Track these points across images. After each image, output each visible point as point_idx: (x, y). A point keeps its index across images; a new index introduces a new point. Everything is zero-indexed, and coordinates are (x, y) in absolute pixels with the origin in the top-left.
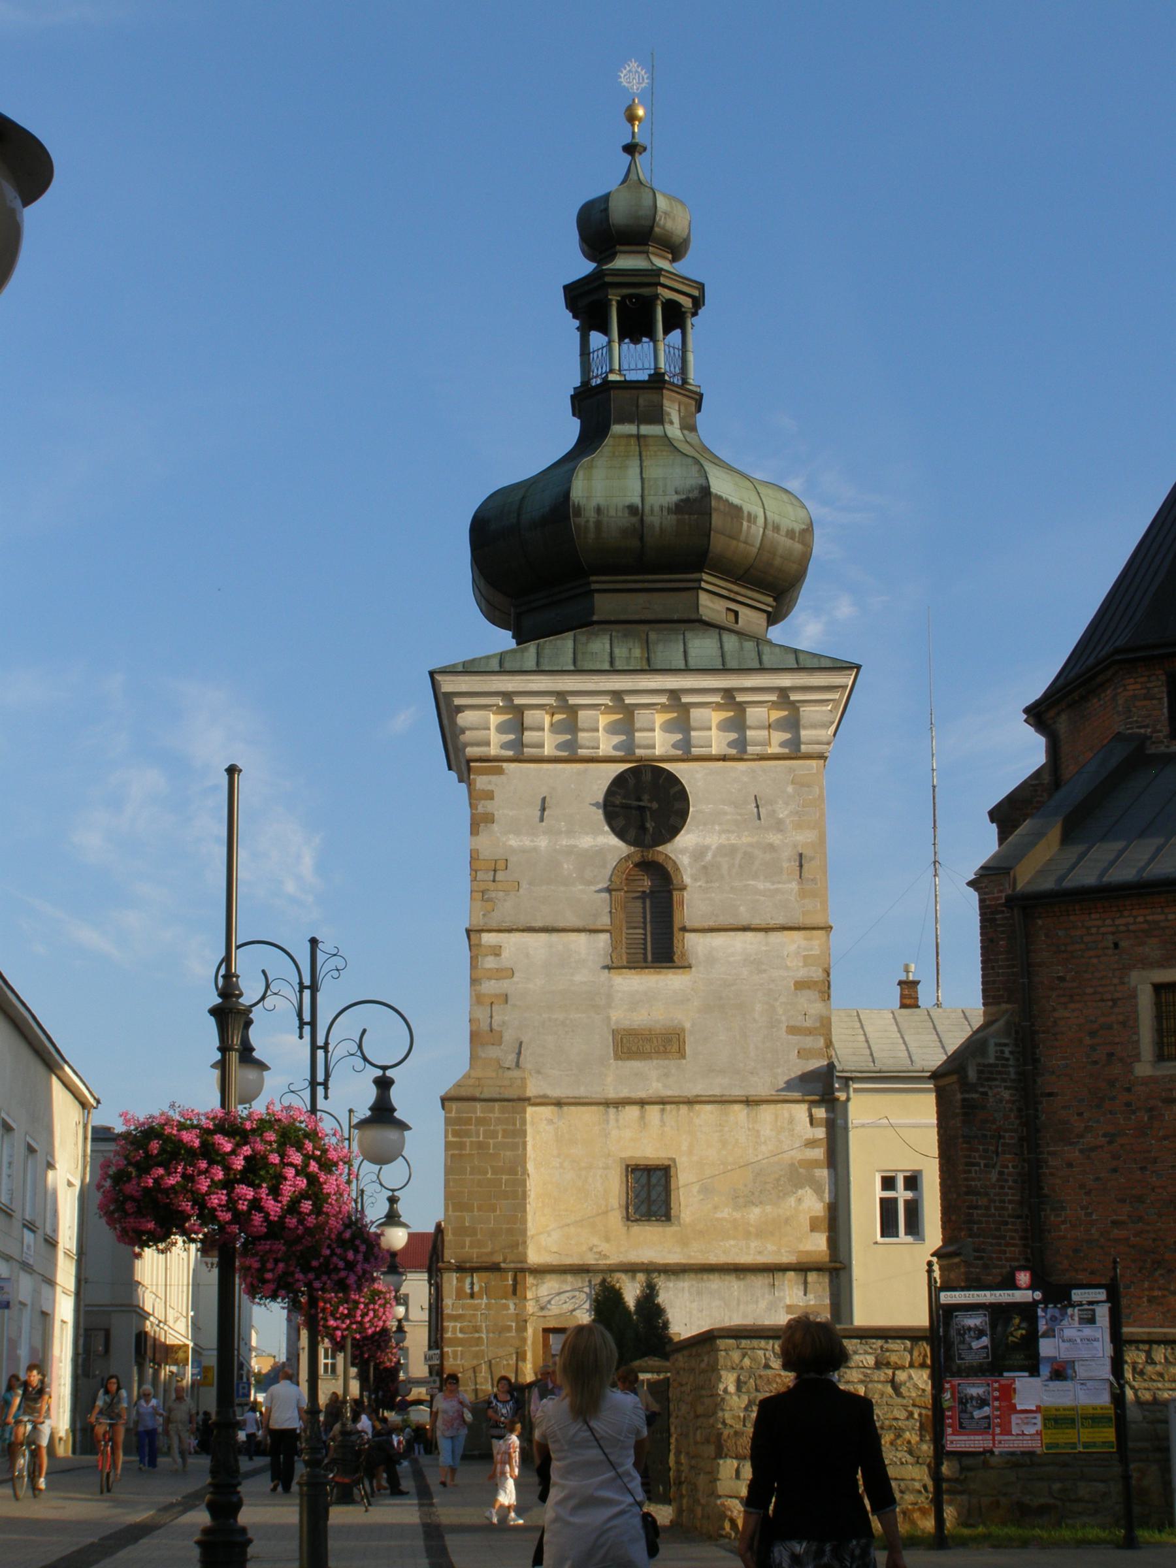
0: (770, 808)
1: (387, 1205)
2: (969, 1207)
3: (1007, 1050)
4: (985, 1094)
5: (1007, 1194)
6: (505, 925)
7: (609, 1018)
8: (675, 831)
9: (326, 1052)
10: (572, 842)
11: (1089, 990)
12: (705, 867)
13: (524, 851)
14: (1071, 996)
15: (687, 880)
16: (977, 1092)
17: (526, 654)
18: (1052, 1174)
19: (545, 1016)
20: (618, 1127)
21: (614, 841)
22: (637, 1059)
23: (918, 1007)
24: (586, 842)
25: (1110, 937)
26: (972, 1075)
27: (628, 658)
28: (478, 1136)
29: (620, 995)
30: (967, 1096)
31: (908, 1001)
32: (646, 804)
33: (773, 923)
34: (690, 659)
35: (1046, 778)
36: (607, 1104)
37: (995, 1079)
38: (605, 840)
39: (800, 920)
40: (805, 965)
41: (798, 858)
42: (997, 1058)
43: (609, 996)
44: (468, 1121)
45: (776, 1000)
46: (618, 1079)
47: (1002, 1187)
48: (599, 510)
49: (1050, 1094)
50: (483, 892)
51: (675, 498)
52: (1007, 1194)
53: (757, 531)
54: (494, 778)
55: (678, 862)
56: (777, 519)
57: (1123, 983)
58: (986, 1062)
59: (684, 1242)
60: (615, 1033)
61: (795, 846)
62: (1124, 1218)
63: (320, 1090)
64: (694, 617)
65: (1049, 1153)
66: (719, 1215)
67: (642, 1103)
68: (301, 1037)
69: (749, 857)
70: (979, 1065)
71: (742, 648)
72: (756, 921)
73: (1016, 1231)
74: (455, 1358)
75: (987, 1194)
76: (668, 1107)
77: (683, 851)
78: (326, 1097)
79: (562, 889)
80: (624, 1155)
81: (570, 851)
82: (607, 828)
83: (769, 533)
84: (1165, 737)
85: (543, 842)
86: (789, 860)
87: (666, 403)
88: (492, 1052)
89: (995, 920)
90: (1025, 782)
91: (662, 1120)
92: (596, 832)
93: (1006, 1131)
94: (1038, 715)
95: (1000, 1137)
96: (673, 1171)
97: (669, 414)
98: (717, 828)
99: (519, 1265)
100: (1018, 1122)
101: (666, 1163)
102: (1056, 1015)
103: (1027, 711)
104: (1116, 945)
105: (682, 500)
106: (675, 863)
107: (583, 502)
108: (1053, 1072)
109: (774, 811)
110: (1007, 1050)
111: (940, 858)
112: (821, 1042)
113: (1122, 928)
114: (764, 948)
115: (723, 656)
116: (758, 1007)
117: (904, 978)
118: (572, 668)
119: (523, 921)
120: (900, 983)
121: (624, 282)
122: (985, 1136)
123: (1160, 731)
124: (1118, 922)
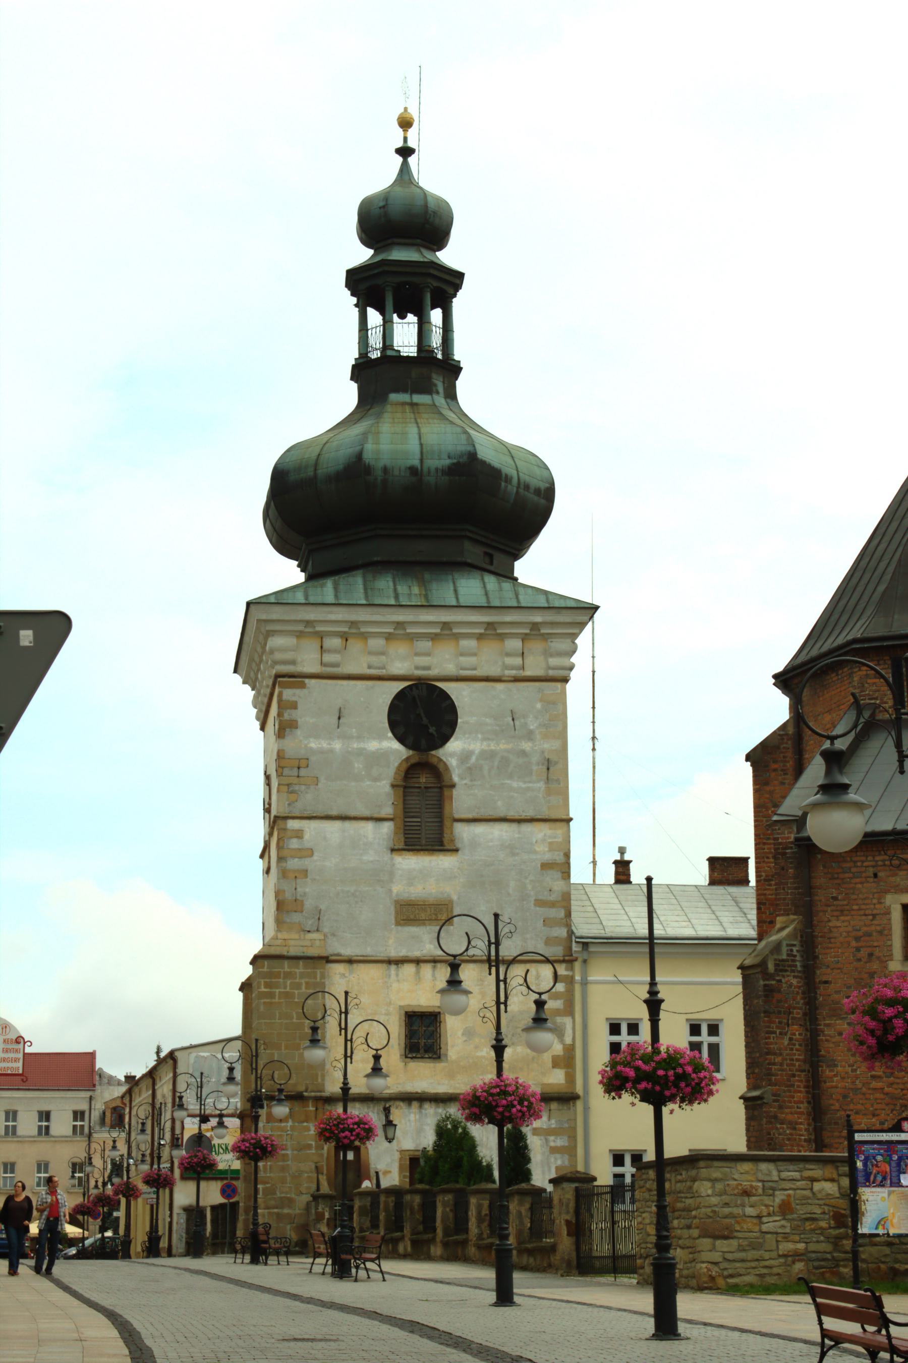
0: (522, 720)
1: (372, 1060)
2: (769, 1064)
3: (795, 949)
4: (780, 981)
5: (795, 1055)
6: (306, 814)
7: (390, 891)
8: (446, 739)
9: (505, 984)
10: (362, 745)
11: (855, 907)
12: (470, 768)
13: (322, 752)
14: (842, 911)
15: (456, 779)
16: (774, 980)
17: (325, 589)
18: (827, 1040)
19: (339, 888)
20: (398, 981)
21: (396, 745)
22: (413, 926)
23: (630, 883)
24: (373, 745)
25: (871, 869)
26: (771, 967)
27: (410, 595)
28: (285, 987)
29: (400, 872)
30: (767, 982)
31: (622, 877)
32: (423, 715)
33: (524, 815)
34: (460, 597)
35: (791, 730)
36: (389, 962)
37: (786, 971)
38: (389, 745)
39: (545, 813)
40: (550, 850)
41: (546, 763)
42: (788, 955)
43: (392, 874)
44: (278, 975)
45: (526, 878)
46: (398, 941)
47: (792, 1049)
48: (385, 470)
49: (826, 982)
50: (288, 785)
51: (447, 462)
52: (795, 1055)
54: (298, 691)
55: (448, 763)
56: (527, 479)
57: (881, 903)
58: (780, 958)
59: (451, 1075)
60: (397, 902)
61: (543, 752)
62: (881, 1073)
63: (349, 1059)
64: (459, 559)
65: (826, 1025)
66: (479, 1054)
67: (418, 962)
68: (490, 974)
69: (505, 761)
70: (775, 960)
71: (501, 589)
72: (512, 814)
73: (801, 1081)
74: (265, 1172)
75: (781, 1054)
76: (439, 965)
77: (452, 755)
78: (506, 1012)
79: (353, 784)
80: (402, 1004)
81: (360, 752)
82: (390, 734)
84: (890, 708)
85: (337, 745)
86: (538, 764)
87: (434, 376)
88: (296, 918)
89: (786, 853)
90: (774, 732)
91: (433, 975)
92: (381, 737)
93: (795, 1008)
94: (784, 680)
95: (790, 1013)
96: (410, 1010)
97: (436, 385)
98: (480, 736)
99: (318, 1094)
100: (802, 1001)
101: (437, 1010)
102: (830, 924)
103: (775, 677)
104: (875, 875)
105: (454, 464)
106: (445, 764)
107: (372, 463)
108: (828, 966)
109: (526, 723)
110: (795, 949)
111: (596, 735)
112: (562, 914)
113: (880, 863)
114: (517, 836)
115: (486, 594)
116: (512, 884)
117: (619, 858)
118: (364, 602)
119: (321, 810)
120: (616, 862)
121: (404, 256)
122: (779, 1012)
123: (886, 703)
124: (877, 858)
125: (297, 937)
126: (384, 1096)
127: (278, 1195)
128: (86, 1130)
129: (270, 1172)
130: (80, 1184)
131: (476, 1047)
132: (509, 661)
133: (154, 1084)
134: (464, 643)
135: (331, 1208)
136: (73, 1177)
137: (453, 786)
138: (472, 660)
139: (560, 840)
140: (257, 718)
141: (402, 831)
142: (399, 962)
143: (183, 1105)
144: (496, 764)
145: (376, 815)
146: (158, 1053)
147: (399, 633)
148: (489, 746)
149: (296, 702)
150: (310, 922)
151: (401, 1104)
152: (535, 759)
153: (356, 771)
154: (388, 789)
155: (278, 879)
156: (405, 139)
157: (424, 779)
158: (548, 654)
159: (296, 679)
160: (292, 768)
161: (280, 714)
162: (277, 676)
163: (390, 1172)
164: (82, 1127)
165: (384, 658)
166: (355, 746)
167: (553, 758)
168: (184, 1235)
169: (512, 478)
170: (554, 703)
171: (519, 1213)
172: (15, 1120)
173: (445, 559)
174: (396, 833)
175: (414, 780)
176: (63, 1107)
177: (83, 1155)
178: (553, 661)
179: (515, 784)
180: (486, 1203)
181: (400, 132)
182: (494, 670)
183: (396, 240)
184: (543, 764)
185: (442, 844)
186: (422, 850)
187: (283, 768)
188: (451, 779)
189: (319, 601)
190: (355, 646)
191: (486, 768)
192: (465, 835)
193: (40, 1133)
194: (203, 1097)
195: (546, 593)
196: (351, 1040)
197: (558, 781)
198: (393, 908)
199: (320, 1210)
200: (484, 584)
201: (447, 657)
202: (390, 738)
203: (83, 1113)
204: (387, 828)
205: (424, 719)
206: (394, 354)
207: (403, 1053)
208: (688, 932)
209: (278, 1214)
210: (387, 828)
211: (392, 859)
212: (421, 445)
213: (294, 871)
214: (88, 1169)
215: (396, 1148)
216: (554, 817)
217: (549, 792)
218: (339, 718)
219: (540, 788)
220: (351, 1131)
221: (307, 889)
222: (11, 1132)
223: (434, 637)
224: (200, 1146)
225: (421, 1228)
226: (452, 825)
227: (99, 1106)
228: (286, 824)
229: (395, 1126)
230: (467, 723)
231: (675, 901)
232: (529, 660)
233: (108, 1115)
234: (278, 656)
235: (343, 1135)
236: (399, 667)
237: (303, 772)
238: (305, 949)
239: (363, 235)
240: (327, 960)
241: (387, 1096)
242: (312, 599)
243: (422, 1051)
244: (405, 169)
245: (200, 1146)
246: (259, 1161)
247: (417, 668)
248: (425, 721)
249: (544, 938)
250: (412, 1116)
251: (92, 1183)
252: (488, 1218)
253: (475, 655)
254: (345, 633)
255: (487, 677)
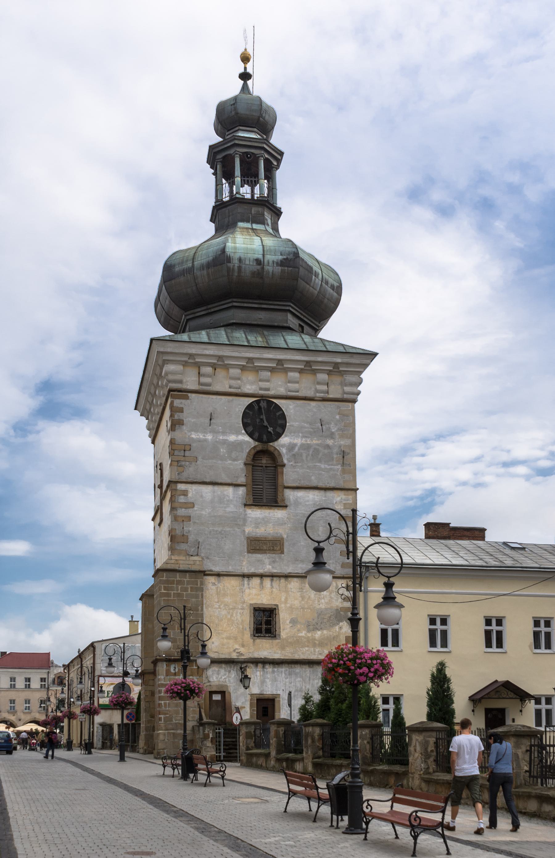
0: (327, 426)
6: (189, 480)
7: (244, 531)
8: (279, 436)
10: (225, 438)
12: (294, 455)
13: (199, 441)
15: (285, 461)
20: (249, 588)
21: (247, 438)
22: (259, 553)
23: (380, 536)
24: (232, 438)
28: (178, 590)
32: (265, 420)
33: (328, 486)
36: (244, 576)
38: (243, 438)
39: (342, 485)
40: (345, 508)
41: (342, 453)
43: (245, 520)
44: (172, 582)
48: (240, 260)
51: (281, 257)
53: (318, 282)
54: (183, 401)
59: (283, 648)
64: (285, 325)
66: (300, 635)
67: (262, 576)
69: (316, 451)
72: (320, 485)
76: (275, 579)
77: (283, 446)
79: (220, 462)
80: (252, 602)
81: (225, 442)
82: (243, 431)
83: (324, 284)
85: (209, 437)
88: (183, 546)
91: (272, 585)
92: (238, 433)
97: (267, 220)
98: (301, 435)
101: (274, 607)
105: (284, 259)
107: (232, 255)
109: (330, 428)
114: (324, 498)
119: (199, 478)
125: (184, 558)
126: (241, 660)
127: (174, 721)
128: (47, 686)
129: (169, 707)
130: (44, 709)
131: (299, 630)
132: (319, 387)
133: (82, 661)
134: (291, 374)
135: (213, 731)
136: (41, 707)
137: (284, 465)
138: (296, 386)
139: (351, 502)
140: (150, 436)
141: (251, 493)
142: (250, 576)
143: (112, 664)
144: (311, 453)
145: (234, 483)
146: (79, 652)
147: (249, 366)
148: (306, 441)
149: (183, 408)
150: (193, 550)
151: (251, 665)
152: (335, 450)
153: (222, 454)
154: (242, 466)
155: (172, 521)
156: (245, 68)
157: (264, 461)
158: (343, 384)
159: (183, 393)
160: (180, 450)
161: (172, 416)
162: (170, 391)
163: (244, 707)
164: (45, 685)
165: (239, 382)
166: (221, 438)
167: (347, 450)
168: (101, 738)
169: (318, 274)
170: (347, 416)
171: (516, 756)
172: (14, 681)
173: (276, 324)
174: (247, 495)
175: (258, 461)
176: (36, 677)
177: (45, 697)
178: (347, 389)
179: (323, 466)
180: (432, 740)
181: (242, 65)
182: (310, 393)
183: (241, 128)
184: (340, 454)
185: (276, 502)
186: (264, 506)
187: (174, 450)
188: (282, 461)
189: (198, 340)
190: (221, 373)
191: (304, 455)
192: (291, 497)
193: (26, 687)
194: (125, 660)
195: (343, 345)
196: (188, 636)
197: (349, 465)
198: (245, 542)
199: (206, 732)
200: (301, 336)
201: (280, 383)
202: (243, 434)
203: (45, 679)
204: (242, 491)
205: (265, 422)
206: (241, 197)
207: (252, 633)
208: (428, 562)
209: (174, 733)
210: (242, 491)
211: (245, 511)
212: (263, 246)
213: (182, 517)
214: (48, 703)
215: (248, 693)
216: (347, 487)
217: (344, 472)
218: (211, 420)
219: (338, 469)
220: (369, 667)
221: (191, 528)
222: (13, 686)
223: (272, 370)
224: (123, 690)
225: (321, 753)
226: (283, 491)
227: (52, 676)
228: (177, 486)
229: (250, 678)
230: (292, 426)
231: (412, 546)
232: (332, 388)
233: (56, 679)
234: (171, 377)
235: (359, 671)
236: (249, 388)
237: (187, 453)
238: (190, 566)
239: (220, 126)
240: (204, 573)
241: (243, 660)
242: (193, 340)
243: (264, 632)
244: (245, 88)
245: (123, 690)
246: (157, 709)
247: (261, 389)
248: (266, 423)
249: (341, 563)
250: (258, 673)
251: (50, 710)
252: (435, 754)
253: (298, 382)
254: (214, 364)
255: (306, 397)
